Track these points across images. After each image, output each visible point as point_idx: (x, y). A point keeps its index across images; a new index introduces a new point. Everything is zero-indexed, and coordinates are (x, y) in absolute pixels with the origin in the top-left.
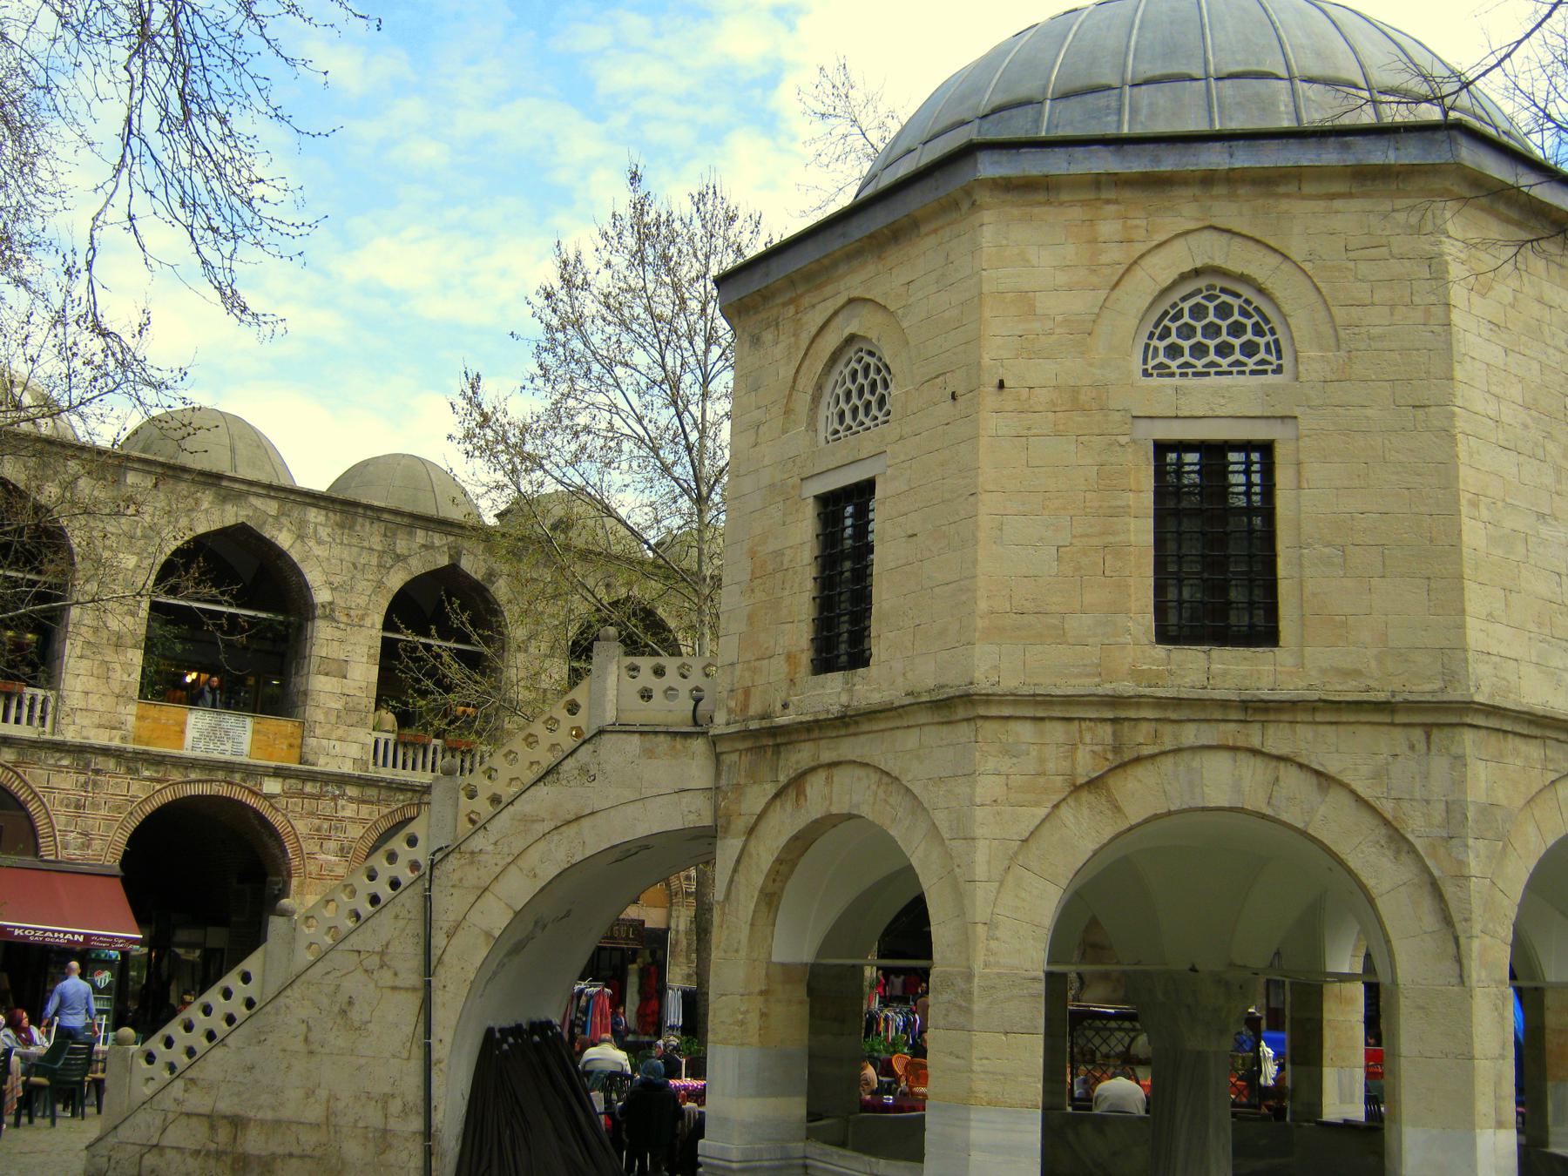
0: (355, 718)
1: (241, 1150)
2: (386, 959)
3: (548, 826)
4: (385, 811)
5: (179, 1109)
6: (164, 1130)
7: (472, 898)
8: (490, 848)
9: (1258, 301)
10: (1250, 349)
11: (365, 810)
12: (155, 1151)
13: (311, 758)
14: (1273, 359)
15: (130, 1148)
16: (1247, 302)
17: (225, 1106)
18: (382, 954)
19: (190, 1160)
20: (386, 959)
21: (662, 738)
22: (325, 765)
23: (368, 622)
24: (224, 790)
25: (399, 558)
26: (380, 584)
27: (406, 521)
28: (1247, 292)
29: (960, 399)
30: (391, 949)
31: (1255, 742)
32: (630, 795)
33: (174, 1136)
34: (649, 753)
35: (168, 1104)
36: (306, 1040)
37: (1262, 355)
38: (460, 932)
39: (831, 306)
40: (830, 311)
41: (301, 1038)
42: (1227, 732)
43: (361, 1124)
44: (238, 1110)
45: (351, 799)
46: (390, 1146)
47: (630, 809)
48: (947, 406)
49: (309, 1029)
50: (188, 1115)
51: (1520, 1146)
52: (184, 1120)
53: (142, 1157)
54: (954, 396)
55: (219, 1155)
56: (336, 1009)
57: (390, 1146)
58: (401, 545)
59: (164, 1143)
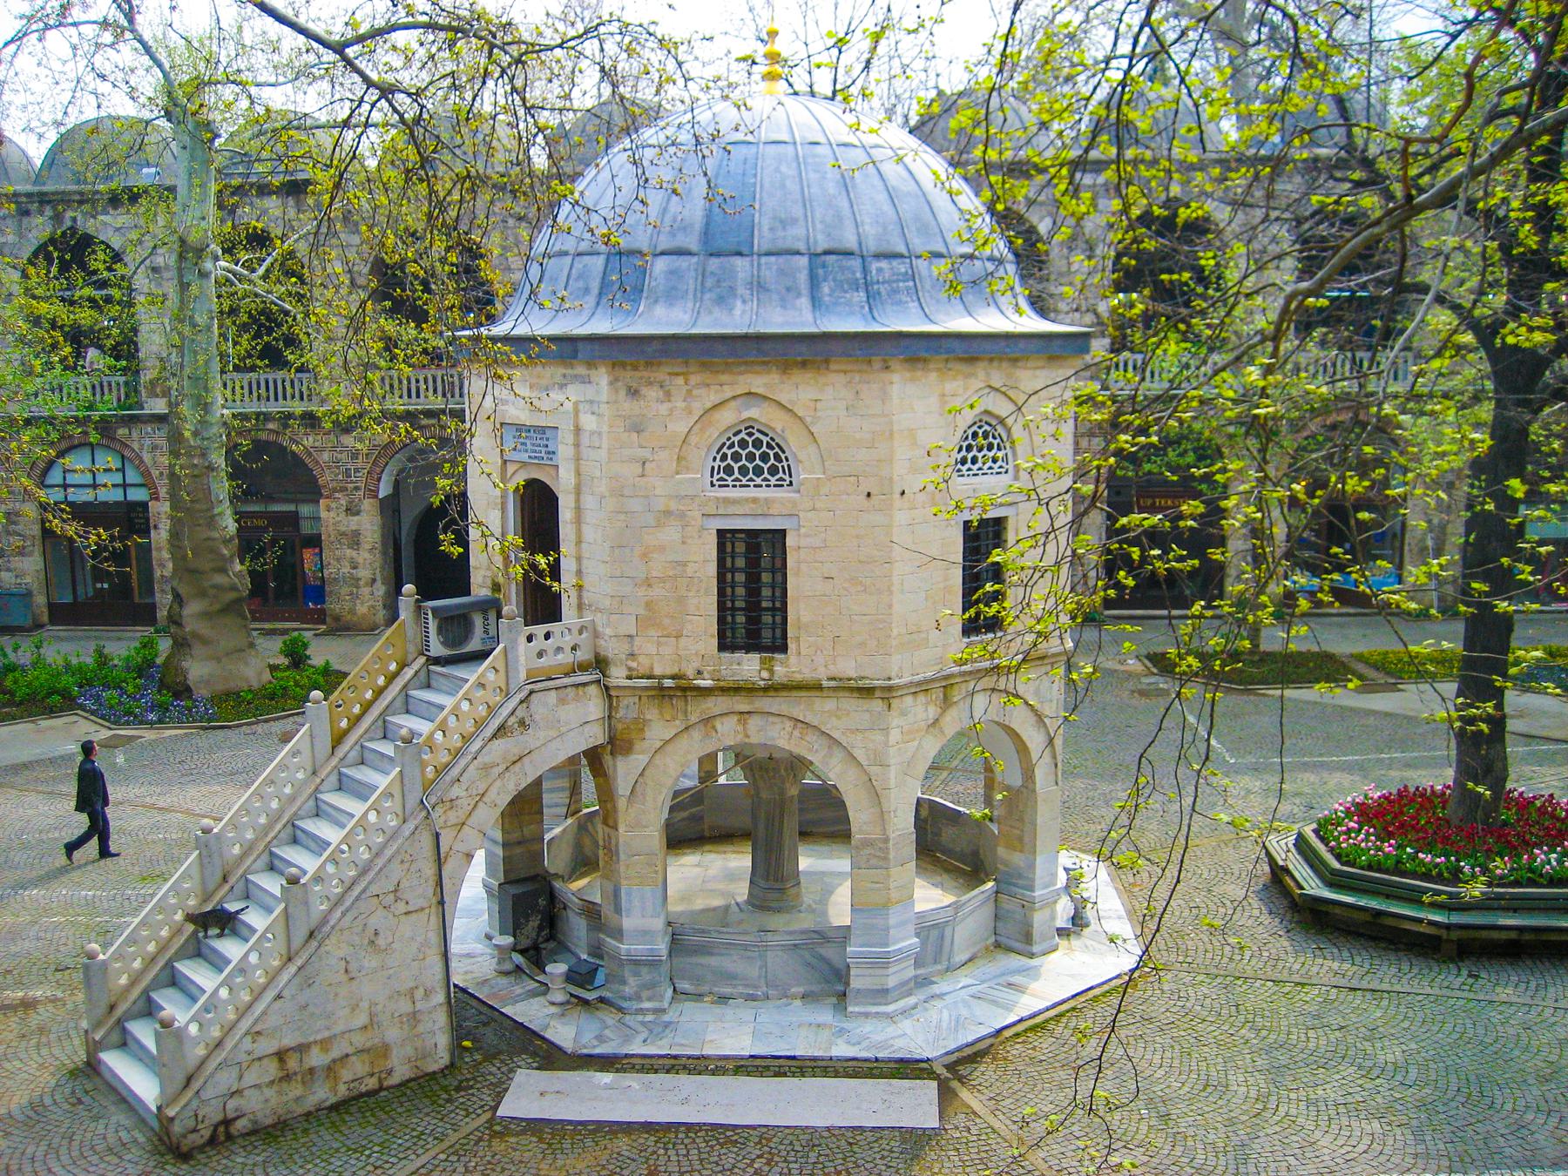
10: (773, 471)
17: (289, 1041)
19: (266, 1090)
33: (251, 1078)
37: (781, 474)
40: (729, 394)
48: (864, 497)
50: (260, 1059)
52: (257, 1064)
54: (869, 495)
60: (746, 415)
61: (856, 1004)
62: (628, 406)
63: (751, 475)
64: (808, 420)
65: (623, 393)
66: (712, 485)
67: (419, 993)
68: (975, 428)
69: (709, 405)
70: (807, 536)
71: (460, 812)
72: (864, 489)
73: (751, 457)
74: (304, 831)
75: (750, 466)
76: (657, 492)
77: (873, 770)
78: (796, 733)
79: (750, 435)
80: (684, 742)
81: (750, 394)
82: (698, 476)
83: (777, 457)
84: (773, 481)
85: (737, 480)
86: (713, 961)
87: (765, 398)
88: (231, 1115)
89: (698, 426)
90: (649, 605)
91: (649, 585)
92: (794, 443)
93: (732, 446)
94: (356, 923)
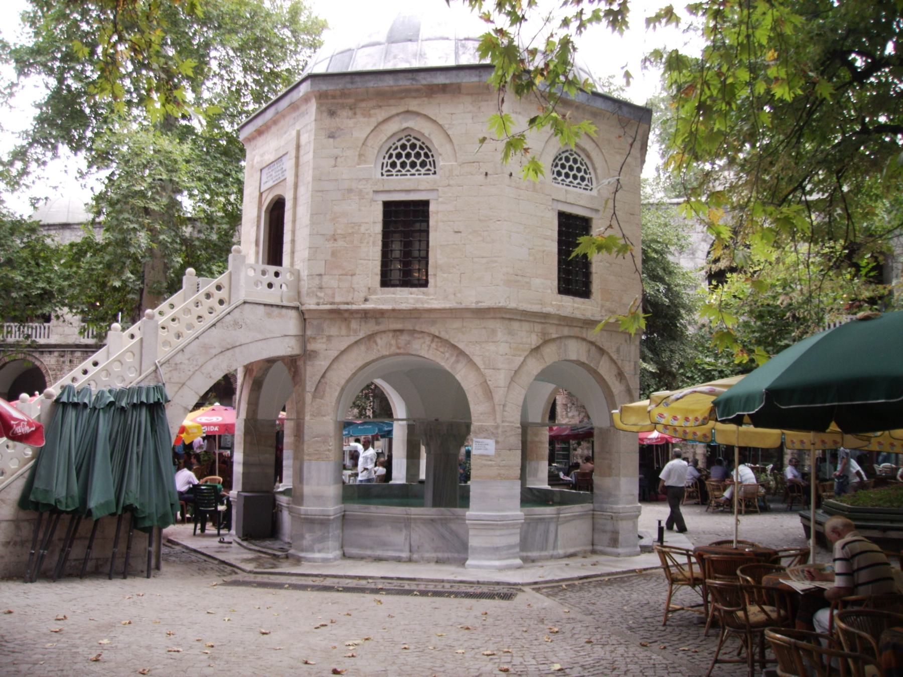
9: (586, 160)
10: (423, 164)
14: (432, 168)
16: (423, 143)
28: (583, 156)
29: (489, 176)
31: (584, 336)
32: (260, 337)
34: (269, 315)
37: (428, 167)
42: (576, 331)
48: (483, 176)
54: (486, 174)
60: (405, 125)
61: (473, 559)
62: (328, 121)
64: (446, 127)
65: (325, 114)
66: (382, 175)
68: (567, 154)
70: (442, 203)
72: (483, 170)
73: (408, 156)
74: (98, 415)
75: (408, 162)
76: (344, 177)
77: (488, 372)
78: (434, 345)
79: (408, 141)
82: (373, 169)
83: (426, 155)
84: (423, 171)
85: (399, 171)
86: (372, 532)
90: (334, 254)
91: (335, 240)
92: (437, 142)
93: (396, 148)
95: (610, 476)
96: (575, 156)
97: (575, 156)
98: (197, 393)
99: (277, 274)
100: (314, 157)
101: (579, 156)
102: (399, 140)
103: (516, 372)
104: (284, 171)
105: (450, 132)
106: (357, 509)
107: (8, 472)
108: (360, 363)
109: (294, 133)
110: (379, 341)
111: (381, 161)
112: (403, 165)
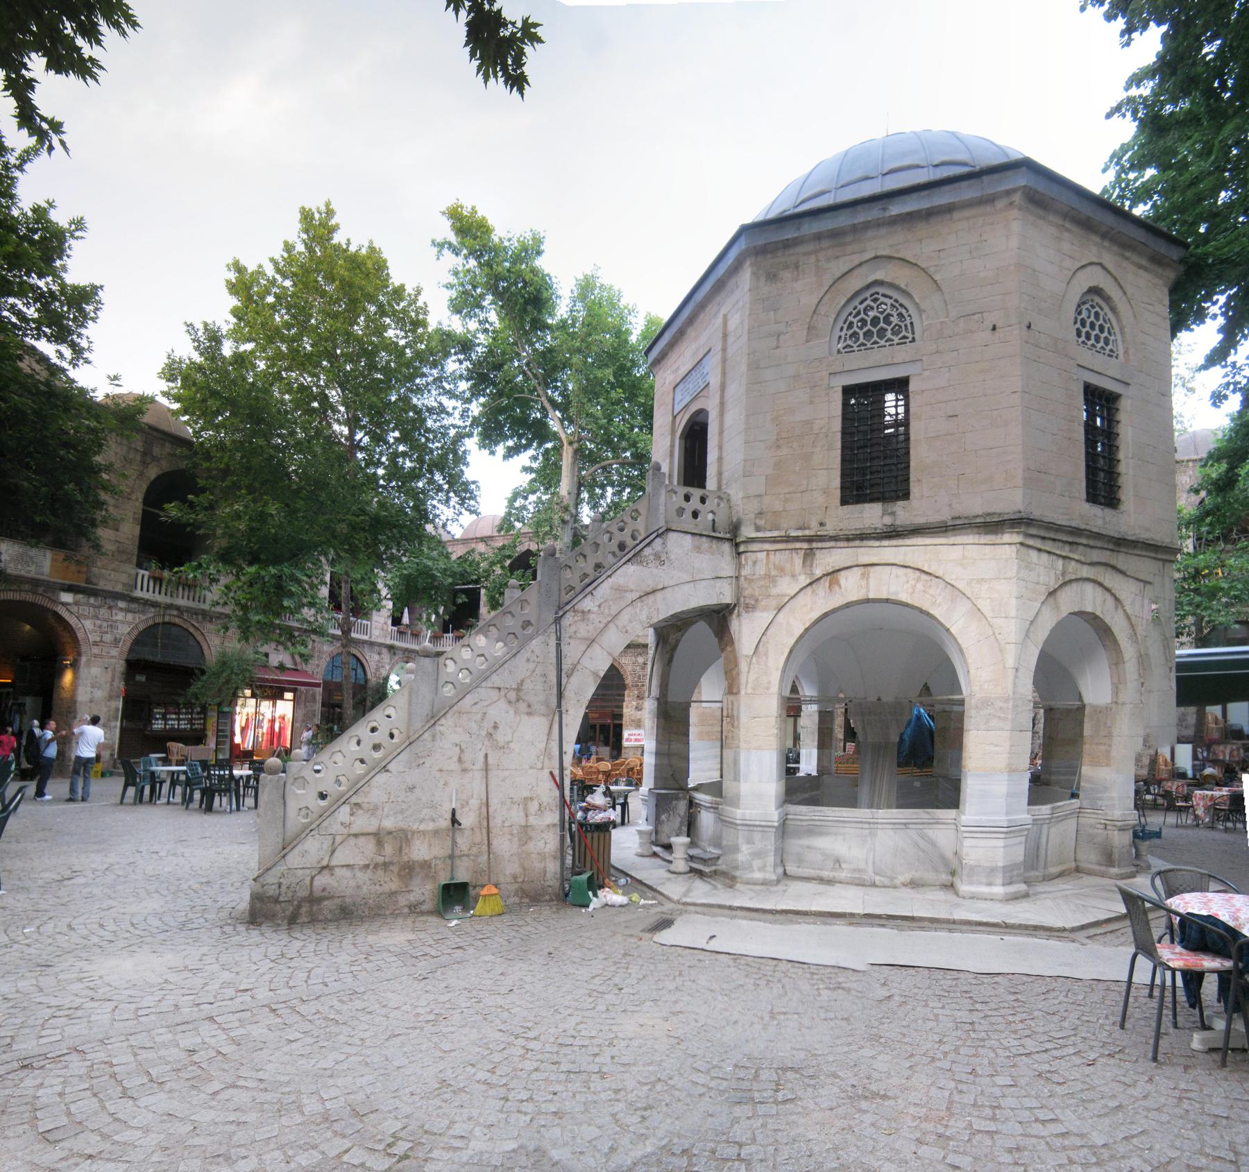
0: (124, 558)
1: (406, 859)
2: (522, 694)
3: (635, 595)
4: (143, 618)
5: (345, 831)
6: (333, 852)
7: (584, 648)
8: (596, 609)
11: (130, 617)
12: (325, 872)
13: (94, 580)
14: (910, 335)
15: (300, 872)
16: (896, 301)
17: (389, 824)
18: (518, 690)
19: (359, 874)
20: (522, 694)
21: (704, 539)
22: (102, 585)
23: (134, 497)
24: (30, 598)
25: (154, 459)
26: (142, 474)
27: (160, 435)
28: (1107, 309)
30: (525, 686)
33: (344, 855)
34: (698, 549)
35: (336, 828)
36: (460, 760)
37: (904, 333)
38: (576, 673)
39: (856, 259)
40: (856, 262)
41: (456, 759)
43: (507, 824)
44: (402, 825)
45: (121, 609)
46: (530, 838)
47: (686, 587)
48: (988, 333)
49: (462, 751)
50: (356, 835)
51: (656, 765)
52: (352, 841)
53: (313, 878)
55: (386, 865)
56: (484, 733)
57: (530, 838)
58: (156, 451)
59: (334, 863)
63: (875, 338)
64: (932, 270)
65: (763, 279)
67: (534, 807)
69: (838, 274)
71: (591, 627)
78: (920, 586)
80: (804, 599)
81: (876, 257)
87: (890, 258)
88: (317, 893)
89: (828, 295)
91: (778, 447)
93: (858, 313)
94: (474, 709)
95: (1108, 765)
96: (1097, 309)
97: (1097, 309)
98: (610, 654)
99: (703, 500)
100: (749, 340)
101: (1102, 309)
102: (861, 303)
103: (1032, 622)
104: (705, 376)
105: (937, 277)
106: (804, 813)
107: (607, 566)
108: (815, 615)
109: (720, 320)
110: (843, 582)
111: (837, 333)
112: (868, 334)
